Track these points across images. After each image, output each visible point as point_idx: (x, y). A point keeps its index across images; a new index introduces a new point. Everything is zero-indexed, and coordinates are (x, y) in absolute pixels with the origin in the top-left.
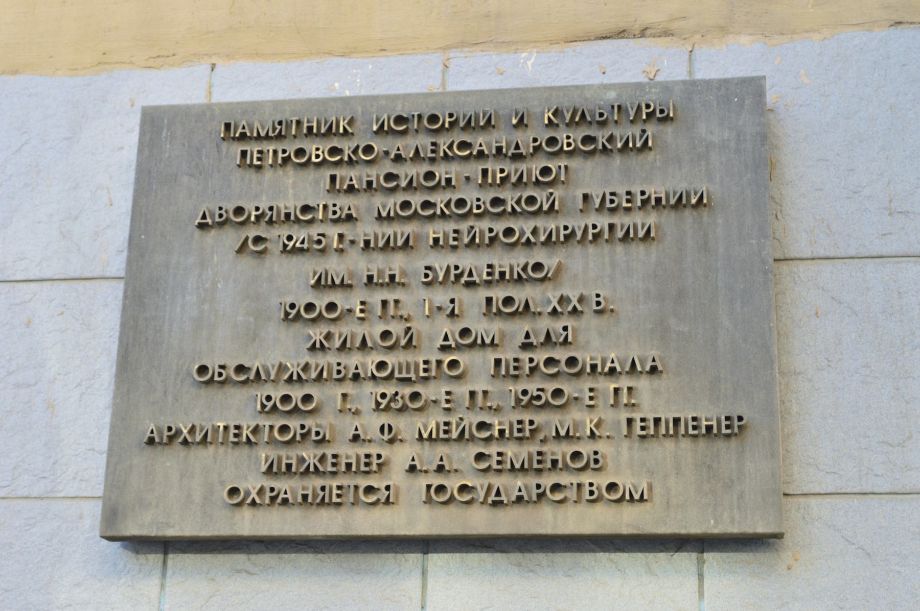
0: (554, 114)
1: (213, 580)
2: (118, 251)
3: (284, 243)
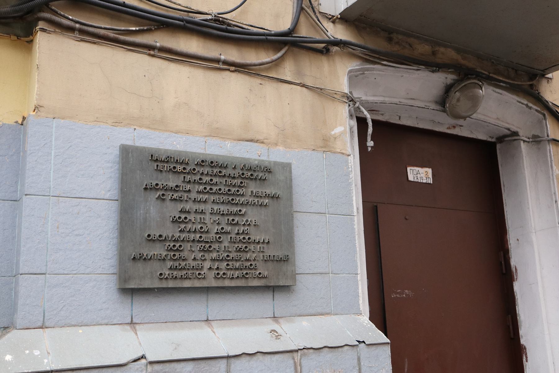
0: (243, 166)
1: (148, 299)
2: (108, 190)
3: (171, 197)
